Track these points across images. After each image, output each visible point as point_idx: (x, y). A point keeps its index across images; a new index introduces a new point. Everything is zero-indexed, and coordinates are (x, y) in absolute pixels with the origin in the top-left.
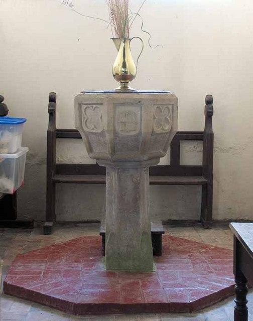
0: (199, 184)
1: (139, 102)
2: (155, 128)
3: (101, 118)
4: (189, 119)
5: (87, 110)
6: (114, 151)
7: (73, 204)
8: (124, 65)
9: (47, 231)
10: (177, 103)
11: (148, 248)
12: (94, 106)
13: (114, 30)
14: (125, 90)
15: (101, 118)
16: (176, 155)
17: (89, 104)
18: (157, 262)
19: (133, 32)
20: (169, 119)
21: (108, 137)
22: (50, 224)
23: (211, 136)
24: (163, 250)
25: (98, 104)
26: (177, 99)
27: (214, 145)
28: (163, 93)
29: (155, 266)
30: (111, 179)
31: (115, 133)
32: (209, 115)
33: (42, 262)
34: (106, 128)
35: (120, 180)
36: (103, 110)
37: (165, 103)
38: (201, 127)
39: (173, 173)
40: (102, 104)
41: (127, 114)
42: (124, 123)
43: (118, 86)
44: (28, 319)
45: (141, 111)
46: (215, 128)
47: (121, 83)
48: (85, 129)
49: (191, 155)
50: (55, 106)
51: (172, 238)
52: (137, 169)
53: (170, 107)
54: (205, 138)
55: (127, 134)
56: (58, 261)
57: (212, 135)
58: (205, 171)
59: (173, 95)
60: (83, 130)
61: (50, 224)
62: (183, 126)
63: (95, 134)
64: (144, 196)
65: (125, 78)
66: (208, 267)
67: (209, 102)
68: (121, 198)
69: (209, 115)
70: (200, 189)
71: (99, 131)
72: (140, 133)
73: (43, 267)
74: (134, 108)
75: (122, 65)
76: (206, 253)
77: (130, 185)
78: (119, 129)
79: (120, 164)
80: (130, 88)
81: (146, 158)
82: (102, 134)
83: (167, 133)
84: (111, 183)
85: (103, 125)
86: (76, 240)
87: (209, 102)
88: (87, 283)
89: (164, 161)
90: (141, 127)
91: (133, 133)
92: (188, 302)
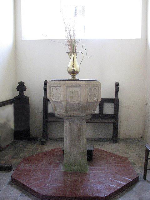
0: (112, 123)
1: (80, 86)
2: (88, 99)
3: (60, 94)
4: (107, 92)
5: (53, 90)
6: (67, 111)
7: (54, 131)
8: (73, 66)
9: (43, 143)
10: (100, 86)
11: (84, 160)
12: (57, 87)
13: (68, 47)
14: (74, 79)
15: (60, 94)
16: (101, 108)
17: (55, 86)
18: (90, 165)
19: (78, 49)
20: (96, 94)
21: (64, 104)
22: (44, 140)
23: (118, 100)
24: (93, 157)
25: (58, 86)
26: (101, 84)
27: (119, 104)
28: (93, 80)
29: (88, 168)
30: (67, 125)
31: (67, 102)
32: (117, 91)
33: (34, 163)
34: (62, 100)
35: (70, 126)
36: (61, 90)
37: (94, 86)
38: (113, 96)
39: (99, 118)
40: (60, 87)
41: (73, 92)
42: (72, 97)
43: (70, 77)
44: (19, 199)
45: (81, 90)
46: (120, 97)
47: (72, 75)
48: (53, 100)
49: (109, 109)
50: (46, 87)
51: (98, 150)
52: (80, 120)
53: (97, 88)
54: (115, 101)
55: (74, 103)
56: (41, 163)
57: (118, 100)
58: (115, 117)
59: (99, 82)
60: (52, 100)
61: (44, 140)
62: (104, 95)
63: (57, 102)
64: (83, 133)
65: (74, 73)
66: (115, 169)
67: (117, 85)
68: (71, 135)
69: (117, 91)
70: (112, 125)
71: (59, 101)
72: (80, 102)
73: (33, 166)
74: (77, 89)
75: (72, 66)
76: (115, 159)
77: (76, 129)
78: (69, 100)
79: (71, 118)
80: (76, 78)
81: (84, 115)
82: (60, 102)
83: (95, 102)
84: (66, 127)
85: (61, 98)
86: (53, 150)
87: (117, 85)
88: (50, 180)
89: (97, 111)
90: (81, 99)
91: (77, 102)
92: (104, 196)
